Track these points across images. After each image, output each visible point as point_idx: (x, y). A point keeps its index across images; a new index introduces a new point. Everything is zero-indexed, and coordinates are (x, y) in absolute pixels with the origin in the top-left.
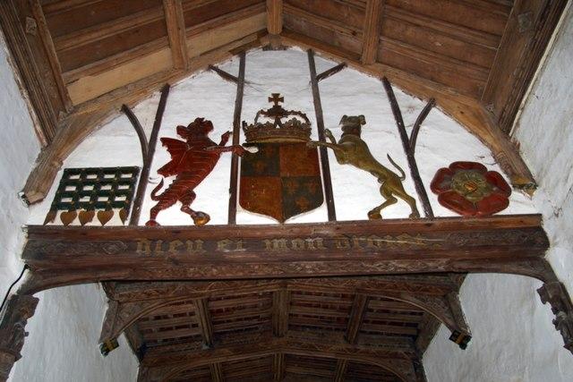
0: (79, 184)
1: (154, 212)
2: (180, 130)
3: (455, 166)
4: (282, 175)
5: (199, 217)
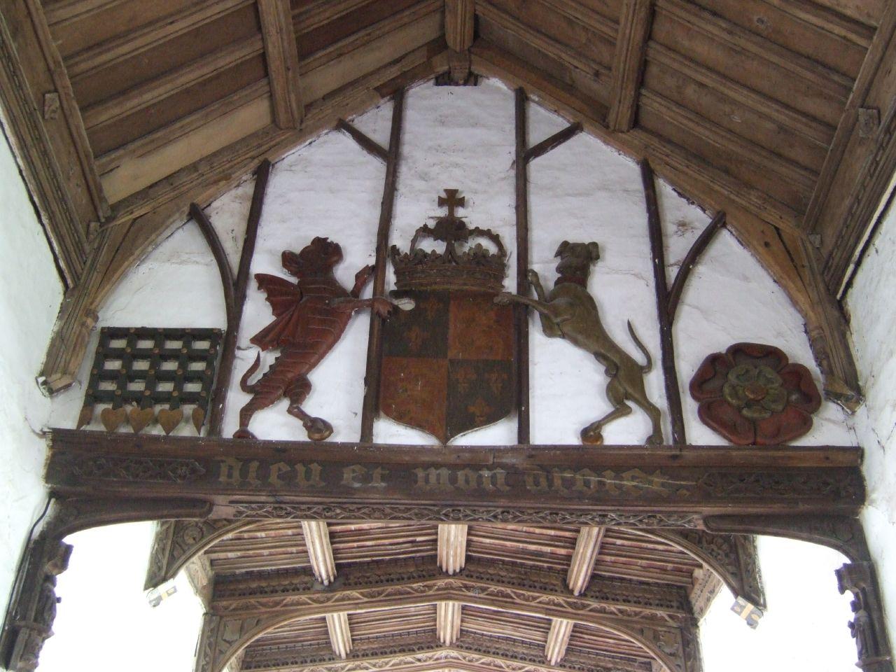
1: (246, 413)
2: (288, 259)
3: (740, 351)
4: (451, 354)
5: (317, 427)
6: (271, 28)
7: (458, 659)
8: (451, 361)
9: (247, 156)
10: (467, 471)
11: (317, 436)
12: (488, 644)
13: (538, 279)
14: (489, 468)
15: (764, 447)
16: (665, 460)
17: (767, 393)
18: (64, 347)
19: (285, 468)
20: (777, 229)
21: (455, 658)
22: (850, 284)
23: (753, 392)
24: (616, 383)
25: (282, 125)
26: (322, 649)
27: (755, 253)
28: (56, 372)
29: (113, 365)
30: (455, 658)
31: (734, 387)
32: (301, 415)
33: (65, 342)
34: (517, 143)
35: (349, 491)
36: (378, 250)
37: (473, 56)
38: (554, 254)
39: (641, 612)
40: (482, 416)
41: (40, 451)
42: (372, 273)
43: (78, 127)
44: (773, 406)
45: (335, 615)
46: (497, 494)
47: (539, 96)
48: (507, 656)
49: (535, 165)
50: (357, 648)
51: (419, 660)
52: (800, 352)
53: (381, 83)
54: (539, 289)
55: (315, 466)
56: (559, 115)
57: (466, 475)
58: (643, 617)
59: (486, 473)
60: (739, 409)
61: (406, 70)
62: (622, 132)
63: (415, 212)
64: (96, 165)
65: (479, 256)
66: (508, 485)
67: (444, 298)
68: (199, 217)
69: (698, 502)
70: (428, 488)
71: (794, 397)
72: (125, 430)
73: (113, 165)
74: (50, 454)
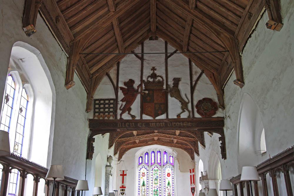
0: (100, 104)
1: (121, 115)
2: (125, 84)
3: (204, 99)
4: (155, 102)
5: (133, 117)
10: (158, 123)
15: (207, 118)
16: (191, 120)
17: (209, 108)
19: (129, 124)
20: (213, 73)
22: (224, 87)
27: (209, 78)
29: (97, 106)
31: (203, 107)
32: (130, 114)
41: (88, 123)
42: (140, 85)
44: (209, 110)
46: (163, 127)
49: (169, 59)
52: (216, 100)
55: (133, 123)
57: (158, 124)
63: (147, 72)
65: (159, 82)
71: (213, 108)
72: (101, 118)
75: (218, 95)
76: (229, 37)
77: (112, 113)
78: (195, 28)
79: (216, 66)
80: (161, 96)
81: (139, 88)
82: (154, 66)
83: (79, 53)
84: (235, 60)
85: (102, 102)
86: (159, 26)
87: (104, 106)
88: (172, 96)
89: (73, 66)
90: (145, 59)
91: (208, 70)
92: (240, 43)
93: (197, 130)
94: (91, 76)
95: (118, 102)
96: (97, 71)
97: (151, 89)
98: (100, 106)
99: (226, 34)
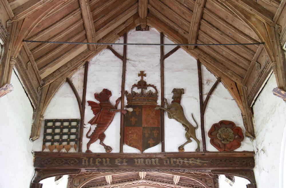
0: (53, 128)
1: (88, 145)
2: (97, 96)
3: (222, 123)
4: (143, 126)
5: (108, 148)
6: (88, 29)
7: (146, 183)
8: (143, 128)
9: (81, 61)
11: (108, 151)
12: (155, 178)
13: (167, 101)
14: (154, 158)
15: (228, 152)
16: (201, 155)
18: (36, 128)
19: (100, 160)
21: (145, 183)
22: (254, 104)
23: (225, 136)
24: (188, 133)
25: (91, 50)
26: (104, 182)
27: (229, 90)
28: (35, 136)
29: (49, 131)
30: (145, 183)
31: (220, 134)
32: (104, 145)
33: (36, 126)
34: (161, 54)
35: (117, 166)
36: (122, 92)
37: (147, 19)
38: (171, 92)
39: (201, 173)
40: (152, 144)
41: (32, 158)
42: (121, 99)
43: (35, 67)
44: (230, 140)
45: (108, 176)
46: (156, 166)
47: (168, 36)
48: (161, 182)
49: (166, 60)
50: (114, 181)
51: (134, 184)
52: (239, 122)
53: (120, 31)
54: (167, 104)
56: (173, 42)
57: (148, 161)
58: (202, 175)
59: (153, 160)
60: (221, 141)
61: (127, 26)
62: (192, 50)
63: (132, 79)
64: (39, 72)
65: (151, 94)
66: (159, 163)
67: (141, 107)
68: (69, 81)
69: (209, 167)
70: (138, 164)
71: (236, 137)
72: (55, 151)
73: (43, 71)
74: (34, 158)
75: (244, 116)
76: (264, 21)
77: (74, 142)
78: (209, 10)
79: (241, 71)
80: (154, 116)
81: (118, 103)
82: (142, 69)
83: (22, 40)
84: (274, 56)
85: (58, 124)
86: (153, 10)
87: (61, 131)
88: (170, 117)
89: (10, 61)
90: (128, 60)
91: (227, 77)
92: (282, 31)
93: (210, 171)
94: (41, 83)
95: (85, 125)
96: (52, 75)
97: (138, 106)
98: (53, 131)
99: (260, 18)
